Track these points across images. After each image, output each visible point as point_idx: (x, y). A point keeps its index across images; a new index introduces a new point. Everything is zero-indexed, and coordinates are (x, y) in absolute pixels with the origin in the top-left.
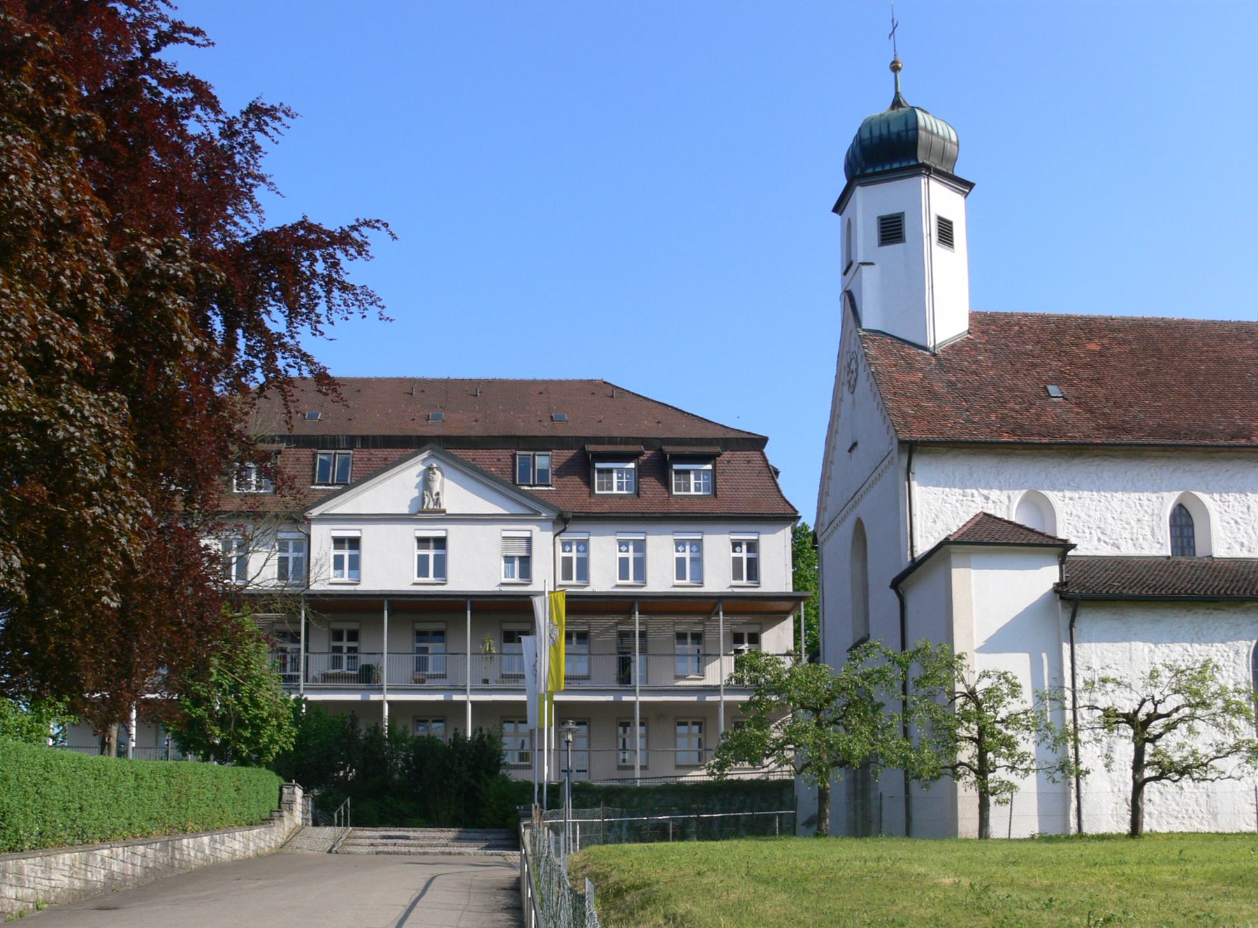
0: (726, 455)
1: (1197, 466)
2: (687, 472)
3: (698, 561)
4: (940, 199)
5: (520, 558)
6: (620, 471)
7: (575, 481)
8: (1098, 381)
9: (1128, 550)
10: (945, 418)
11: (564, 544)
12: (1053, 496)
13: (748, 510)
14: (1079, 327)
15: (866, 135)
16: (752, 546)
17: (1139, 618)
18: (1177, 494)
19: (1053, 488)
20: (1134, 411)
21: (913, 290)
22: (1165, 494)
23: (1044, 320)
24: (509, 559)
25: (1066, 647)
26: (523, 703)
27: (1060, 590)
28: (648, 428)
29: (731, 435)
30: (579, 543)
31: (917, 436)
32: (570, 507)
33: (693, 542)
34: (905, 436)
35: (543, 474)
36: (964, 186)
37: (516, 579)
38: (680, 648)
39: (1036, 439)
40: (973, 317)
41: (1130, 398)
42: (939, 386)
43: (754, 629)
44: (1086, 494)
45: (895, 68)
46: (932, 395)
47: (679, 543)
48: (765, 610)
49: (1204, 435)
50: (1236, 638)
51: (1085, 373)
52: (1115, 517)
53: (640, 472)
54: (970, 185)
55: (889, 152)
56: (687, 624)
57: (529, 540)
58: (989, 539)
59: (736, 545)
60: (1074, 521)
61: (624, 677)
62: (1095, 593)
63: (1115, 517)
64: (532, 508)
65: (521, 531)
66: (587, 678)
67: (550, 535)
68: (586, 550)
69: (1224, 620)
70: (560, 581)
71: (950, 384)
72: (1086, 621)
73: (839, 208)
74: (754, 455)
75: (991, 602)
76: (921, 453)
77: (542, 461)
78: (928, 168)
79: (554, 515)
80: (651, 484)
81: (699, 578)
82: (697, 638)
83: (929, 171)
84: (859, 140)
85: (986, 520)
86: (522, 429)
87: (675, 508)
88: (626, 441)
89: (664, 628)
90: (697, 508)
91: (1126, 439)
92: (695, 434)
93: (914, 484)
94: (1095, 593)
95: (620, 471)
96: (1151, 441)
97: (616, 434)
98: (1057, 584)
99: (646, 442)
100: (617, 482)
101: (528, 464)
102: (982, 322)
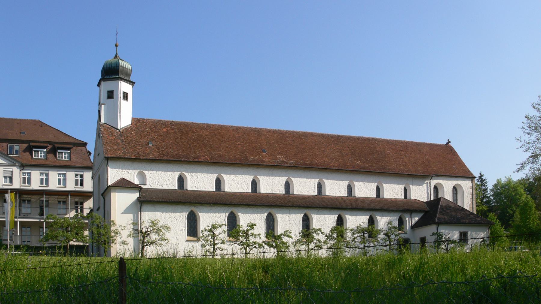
0: (74, 148)
1: (185, 166)
2: (62, 153)
3: (65, 180)
4: (124, 87)
5: (9, 177)
6: (41, 151)
7: (28, 154)
8: (163, 141)
9: (165, 187)
10: (119, 150)
11: (23, 173)
12: (146, 172)
13: (80, 165)
14: (162, 124)
15: (105, 67)
16: (82, 176)
17: (158, 207)
18: (179, 173)
19: (146, 170)
20: (171, 150)
21: (114, 112)
22: (176, 173)
23: (153, 121)
24: (5, 177)
25: (139, 213)
26: (5, 221)
27: (139, 199)
28: (51, 138)
29: (76, 142)
30: (28, 173)
31: (110, 156)
32: (25, 162)
33: (63, 174)
34: (107, 155)
35: (17, 152)
36: (132, 83)
37: (8, 183)
38: (59, 206)
39: (141, 158)
40: (133, 119)
41: (171, 146)
42: (119, 141)
43: (82, 201)
44: (155, 172)
45: (116, 46)
46: (116, 143)
47: (59, 174)
48: (86, 195)
49: (187, 158)
50: (183, 212)
51: (160, 138)
52: (162, 179)
53: (48, 153)
54: (134, 83)
55: (111, 72)
56: (61, 199)
57: (12, 172)
58: (124, 185)
59: (76, 175)
60: (151, 179)
61: (41, 214)
62: (149, 199)
63: (162, 179)
64: (13, 162)
65: (9, 169)
66: (30, 214)
67: (19, 170)
68: (30, 175)
69: (180, 207)
70: (22, 184)
71: (123, 140)
72: (144, 207)
73: (99, 85)
74: (83, 148)
75: (121, 201)
76: (111, 160)
77: (16, 147)
78: (121, 78)
79: (20, 165)
80: (51, 156)
81: (65, 185)
82: (64, 202)
83: (122, 79)
84: (104, 68)
85: (123, 180)
86: (10, 137)
87: (58, 164)
88: (43, 142)
89: (53, 200)
90: (64, 164)
91: (165, 158)
92: (65, 141)
93: (109, 168)
94: (149, 199)
95: (41, 151)
96: (172, 159)
97: (41, 140)
98: (138, 198)
99: (50, 143)
100: (40, 155)
101: (12, 148)
102: (136, 121)
